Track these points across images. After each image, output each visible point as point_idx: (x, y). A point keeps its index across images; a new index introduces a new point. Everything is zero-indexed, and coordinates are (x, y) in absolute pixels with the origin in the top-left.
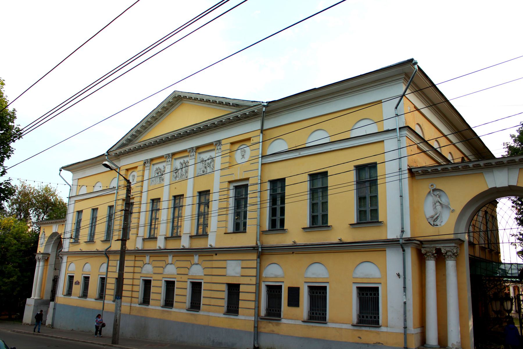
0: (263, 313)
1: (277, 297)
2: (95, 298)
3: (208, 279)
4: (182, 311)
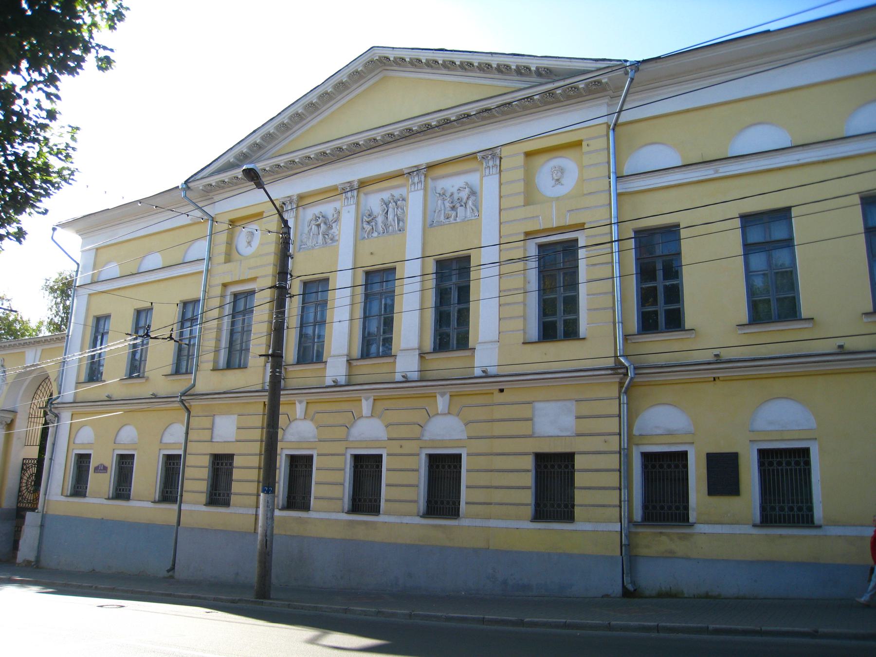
0: (638, 515)
1: (667, 479)
2: (153, 500)
3: (395, 447)
4: (406, 520)
